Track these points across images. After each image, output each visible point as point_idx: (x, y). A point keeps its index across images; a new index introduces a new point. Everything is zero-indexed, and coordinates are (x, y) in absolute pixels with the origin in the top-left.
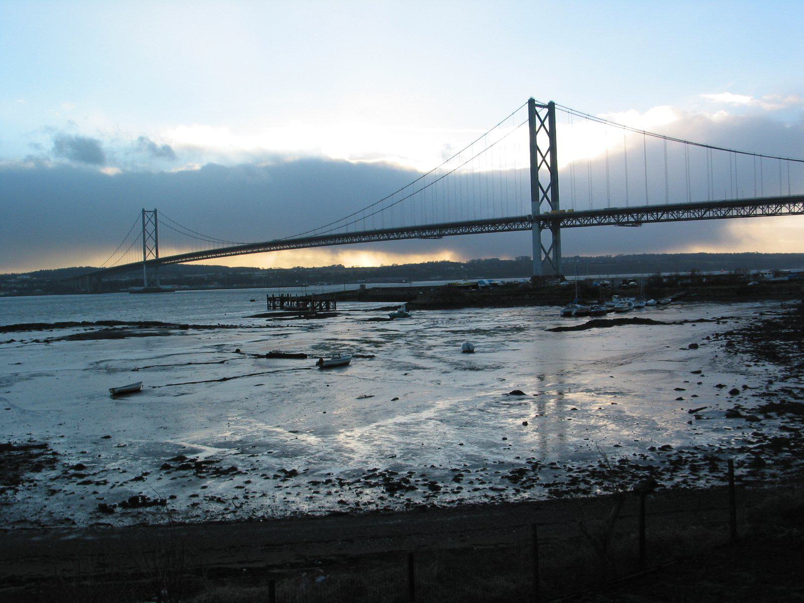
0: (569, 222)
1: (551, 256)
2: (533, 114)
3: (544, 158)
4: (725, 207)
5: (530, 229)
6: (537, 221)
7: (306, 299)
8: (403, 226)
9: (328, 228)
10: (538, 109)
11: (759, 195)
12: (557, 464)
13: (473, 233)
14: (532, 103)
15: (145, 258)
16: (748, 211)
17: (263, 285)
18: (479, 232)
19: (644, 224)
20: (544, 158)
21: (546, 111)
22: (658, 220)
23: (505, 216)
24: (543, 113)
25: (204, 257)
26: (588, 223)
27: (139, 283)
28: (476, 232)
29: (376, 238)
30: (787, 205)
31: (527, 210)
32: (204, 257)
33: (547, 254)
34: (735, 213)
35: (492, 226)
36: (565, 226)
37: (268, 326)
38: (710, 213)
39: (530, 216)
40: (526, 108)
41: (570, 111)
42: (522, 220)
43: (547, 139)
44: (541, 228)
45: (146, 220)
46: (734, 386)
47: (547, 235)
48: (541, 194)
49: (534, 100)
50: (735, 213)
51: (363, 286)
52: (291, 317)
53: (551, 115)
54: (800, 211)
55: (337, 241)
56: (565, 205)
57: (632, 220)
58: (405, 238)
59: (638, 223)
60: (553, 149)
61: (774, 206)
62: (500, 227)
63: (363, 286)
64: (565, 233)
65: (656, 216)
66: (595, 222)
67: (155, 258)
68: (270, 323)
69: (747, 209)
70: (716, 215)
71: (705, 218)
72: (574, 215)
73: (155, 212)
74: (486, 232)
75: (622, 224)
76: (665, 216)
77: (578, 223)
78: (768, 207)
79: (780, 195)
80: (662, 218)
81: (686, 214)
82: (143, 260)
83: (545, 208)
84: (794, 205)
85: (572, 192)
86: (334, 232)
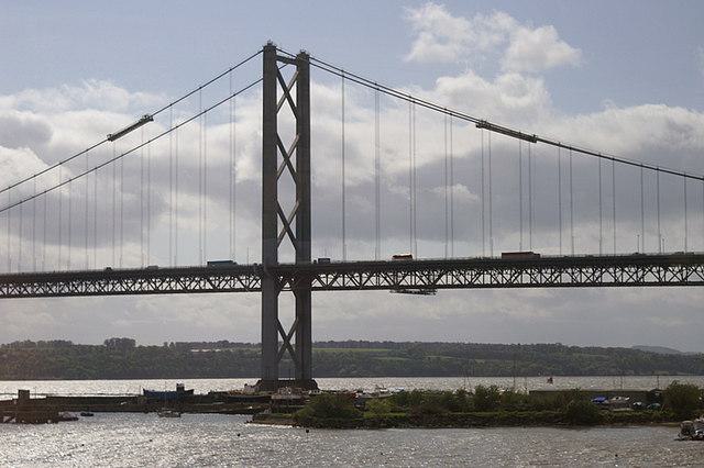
0: (165, 285)
1: (293, 341)
2: (271, 77)
5: (257, 290)
6: (270, 276)
14: (270, 52)
16: (548, 276)
17: (613, 370)
18: (16, 296)
22: (361, 287)
24: (288, 72)
26: (197, 288)
30: (611, 270)
31: (252, 255)
34: (487, 279)
35: (40, 286)
38: (446, 279)
49: (274, 48)
50: (487, 279)
53: (303, 82)
54: (631, 280)
59: (429, 289)
61: (591, 270)
62: (54, 289)
65: (358, 279)
66: (238, 285)
69: (547, 273)
70: (457, 283)
72: (326, 266)
74: (28, 296)
77: (208, 286)
78: (540, 272)
83: (287, 255)
84: (666, 270)
85: (171, 233)
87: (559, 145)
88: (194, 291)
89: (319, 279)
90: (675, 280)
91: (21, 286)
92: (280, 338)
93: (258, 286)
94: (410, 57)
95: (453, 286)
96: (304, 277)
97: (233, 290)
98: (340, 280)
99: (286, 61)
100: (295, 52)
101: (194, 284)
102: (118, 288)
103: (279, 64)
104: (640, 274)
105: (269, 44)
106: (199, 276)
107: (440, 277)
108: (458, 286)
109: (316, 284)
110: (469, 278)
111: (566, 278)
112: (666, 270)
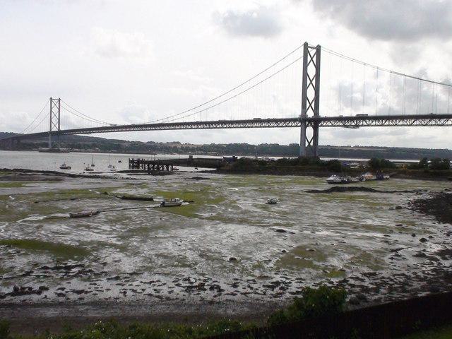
1: (312, 144)
2: (306, 52)
3: (311, 82)
4: (427, 118)
6: (303, 121)
7: (153, 163)
8: (403, 114)
10: (309, 49)
12: (174, 286)
13: (263, 127)
14: (306, 45)
19: (360, 128)
20: (311, 82)
21: (315, 50)
23: (232, 119)
24: (313, 52)
27: (46, 145)
28: (265, 127)
29: (201, 126)
33: (309, 143)
36: (322, 126)
37: (127, 178)
38: (417, 122)
40: (302, 49)
41: (331, 52)
42: (294, 120)
43: (309, 72)
45: (53, 105)
46: (69, 283)
47: (310, 131)
48: (308, 105)
51: (191, 157)
52: (209, 169)
55: (177, 127)
56: (322, 114)
57: (353, 124)
59: (357, 126)
60: (317, 76)
63: (191, 157)
68: (128, 176)
69: (442, 121)
71: (429, 125)
73: (59, 100)
75: (347, 127)
76: (387, 123)
83: (310, 114)
96: (316, 122)
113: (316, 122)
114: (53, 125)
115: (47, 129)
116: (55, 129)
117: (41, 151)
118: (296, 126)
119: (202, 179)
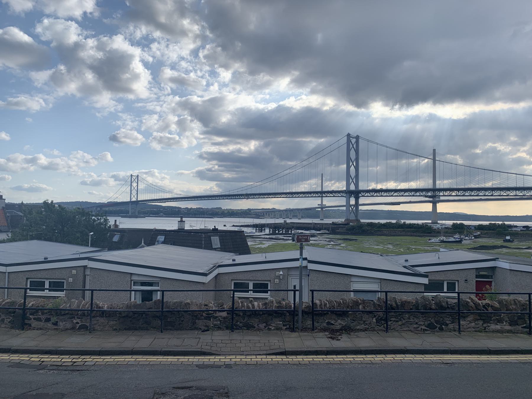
2: (349, 141)
6: (349, 193)
9: (233, 191)
11: (276, 192)
15: (131, 199)
18: (291, 197)
24: (353, 141)
25: (186, 200)
32: (186, 200)
36: (363, 196)
39: (345, 191)
44: (350, 196)
47: (353, 201)
53: (357, 142)
55: (213, 198)
58: (252, 198)
59: (165, 202)
61: (449, 192)
63: (285, 221)
64: (362, 201)
67: (136, 200)
69: (424, 193)
71: (394, 196)
73: (138, 176)
74: (294, 197)
79: (523, 186)
80: (374, 195)
81: (385, 194)
82: (129, 201)
83: (352, 187)
84: (459, 192)
86: (234, 193)
87: (484, 169)
88: (328, 197)
89: (361, 194)
90: (461, 195)
91: (286, 195)
92: (351, 209)
93: (345, 196)
94: (133, 105)
95: (397, 196)
96: (357, 194)
97: (338, 197)
98: (367, 194)
99: (353, 138)
100: (355, 135)
101: (328, 195)
102: (310, 196)
103: (351, 139)
104: (464, 193)
105: (349, 134)
106: (449, 191)
107: (394, 193)
108: (420, 196)
109: (360, 195)
110: (402, 194)
111: (418, 194)
112: (459, 192)
113: (357, 194)
114: (132, 196)
115: (129, 200)
116: (134, 199)
117: (218, 217)
118: (319, 197)
119: (510, 248)
